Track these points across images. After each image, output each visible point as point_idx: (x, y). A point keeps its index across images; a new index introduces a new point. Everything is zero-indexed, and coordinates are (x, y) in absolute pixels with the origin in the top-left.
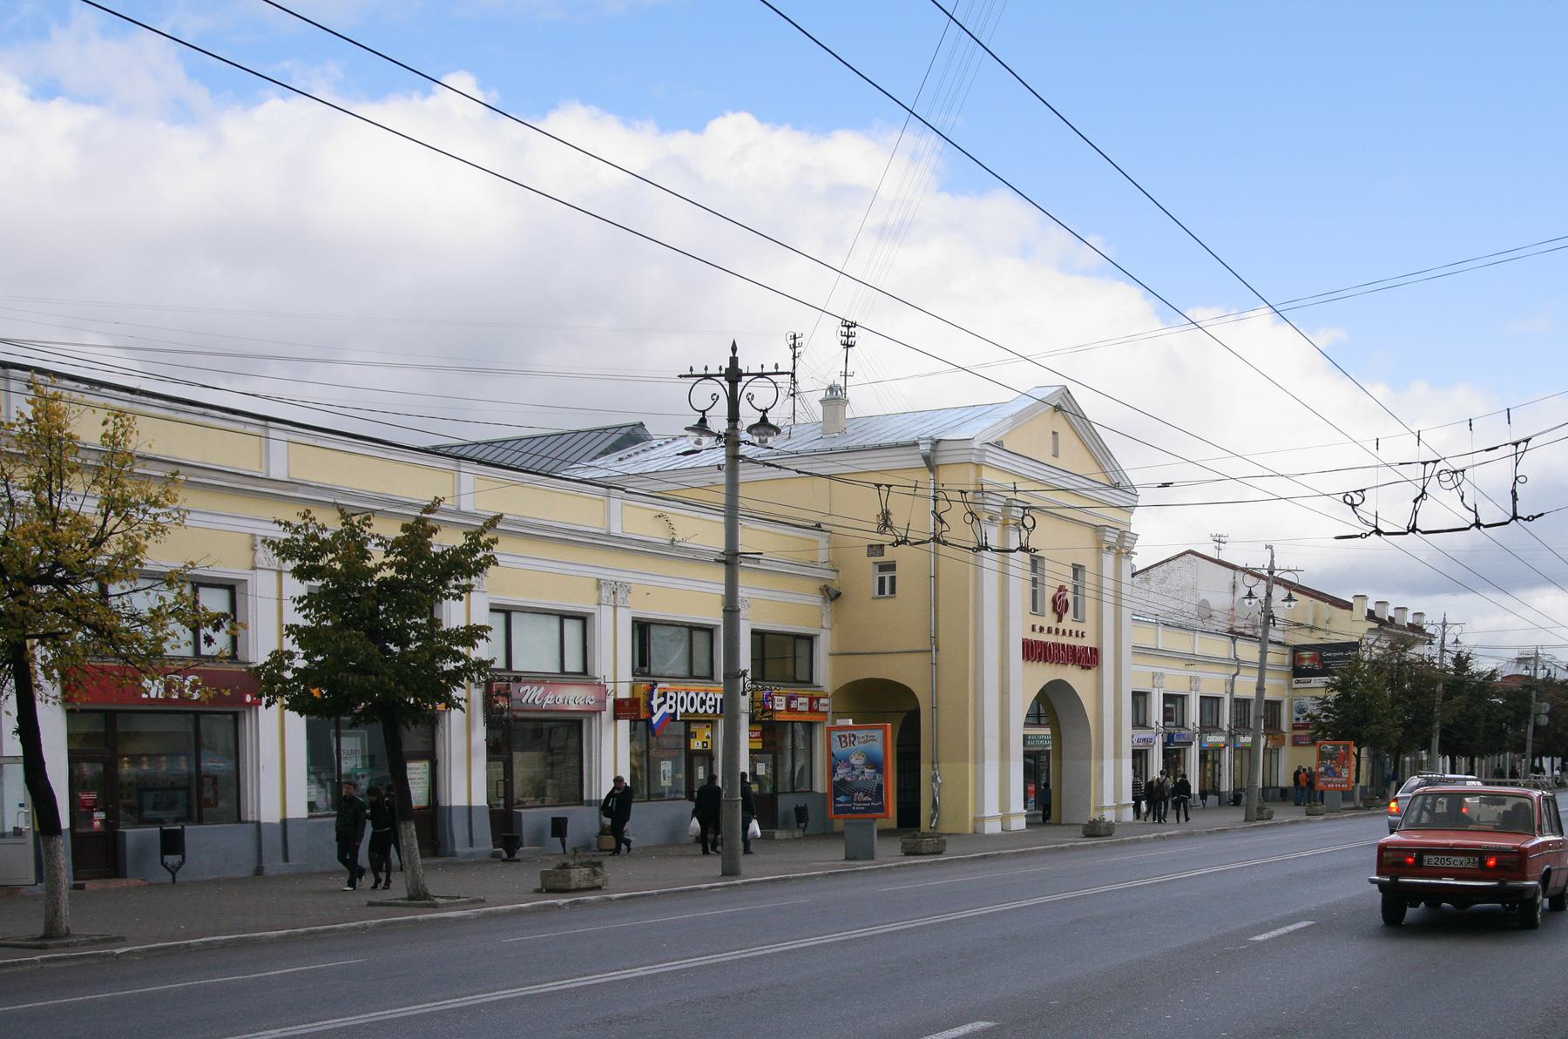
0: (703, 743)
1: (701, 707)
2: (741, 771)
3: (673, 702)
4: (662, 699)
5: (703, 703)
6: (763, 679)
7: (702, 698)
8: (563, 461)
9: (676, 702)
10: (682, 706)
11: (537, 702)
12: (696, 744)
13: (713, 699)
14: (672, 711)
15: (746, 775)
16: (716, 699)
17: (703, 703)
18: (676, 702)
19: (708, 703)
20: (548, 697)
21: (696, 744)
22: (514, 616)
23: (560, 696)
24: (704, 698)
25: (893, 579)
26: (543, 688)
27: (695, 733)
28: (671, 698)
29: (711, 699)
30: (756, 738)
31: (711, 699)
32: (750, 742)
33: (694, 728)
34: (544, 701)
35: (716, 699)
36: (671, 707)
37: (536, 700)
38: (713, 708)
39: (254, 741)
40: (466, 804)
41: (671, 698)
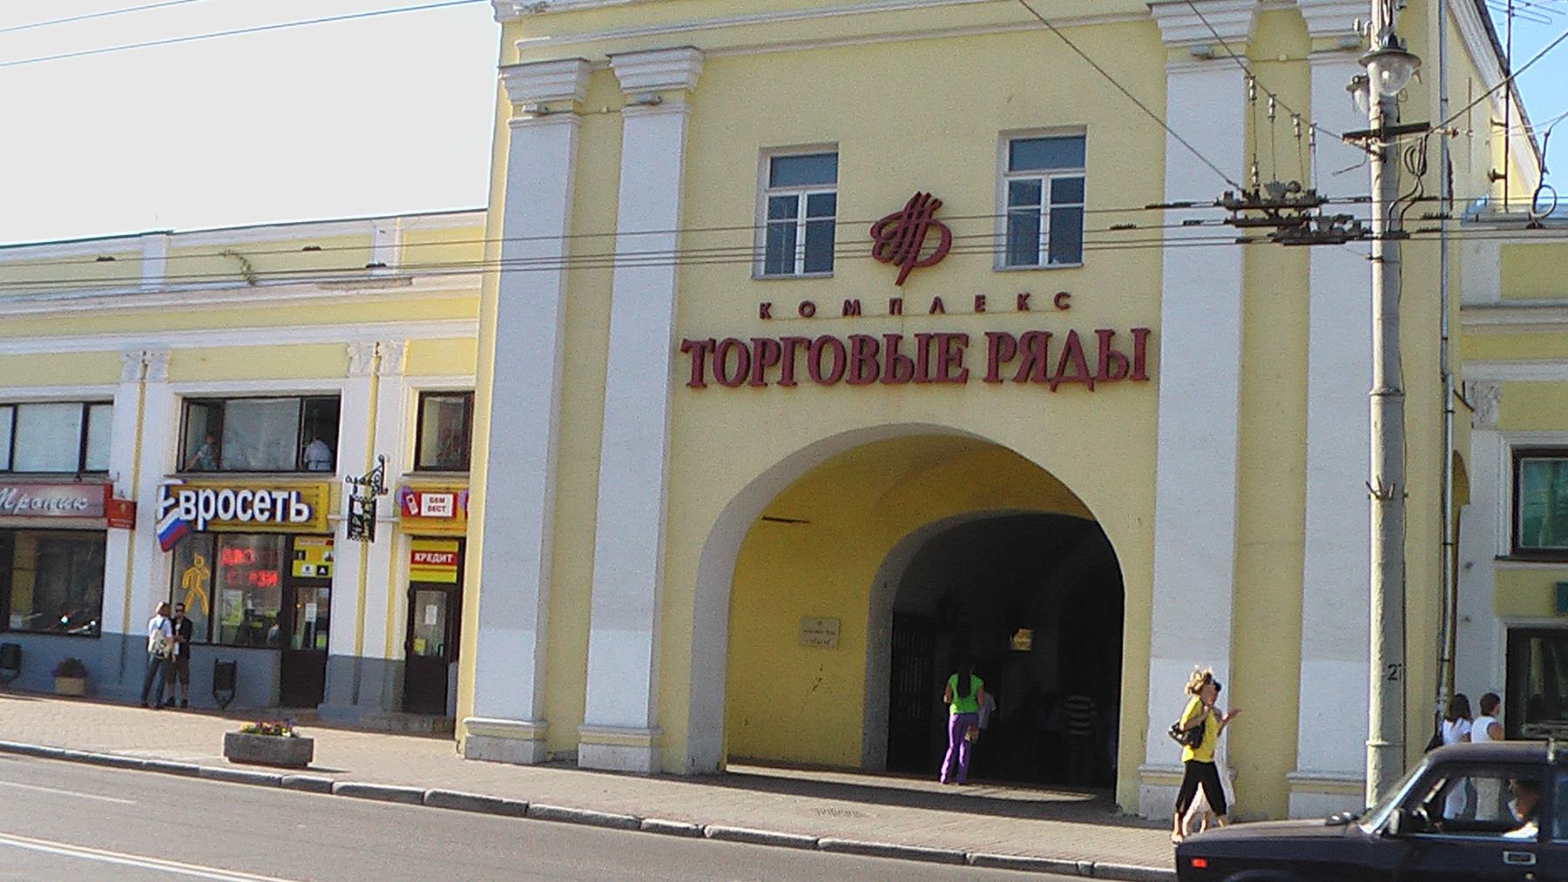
0: (319, 568)
1: (244, 511)
2: (307, 620)
3: (191, 505)
4: (172, 501)
5: (246, 505)
6: (216, 466)
7: (245, 499)
8: (1233, 56)
9: (196, 505)
10: (207, 509)
11: (7, 506)
12: (302, 569)
13: (268, 500)
14: (191, 517)
15: (1498, 699)
16: (274, 502)
17: (246, 505)
18: (196, 505)
19: (257, 505)
20: (21, 501)
21: (302, 569)
22: (22, 411)
23: (39, 501)
24: (250, 498)
25: (1070, 191)
26: (15, 490)
27: (304, 553)
28: (188, 499)
29: (262, 500)
30: (446, 563)
31: (262, 500)
32: (412, 570)
33: (299, 544)
34: (15, 506)
35: (274, 502)
36: (188, 511)
37: (7, 503)
38: (267, 514)
39: (1450, 565)
40: (121, 632)
41: (188, 499)
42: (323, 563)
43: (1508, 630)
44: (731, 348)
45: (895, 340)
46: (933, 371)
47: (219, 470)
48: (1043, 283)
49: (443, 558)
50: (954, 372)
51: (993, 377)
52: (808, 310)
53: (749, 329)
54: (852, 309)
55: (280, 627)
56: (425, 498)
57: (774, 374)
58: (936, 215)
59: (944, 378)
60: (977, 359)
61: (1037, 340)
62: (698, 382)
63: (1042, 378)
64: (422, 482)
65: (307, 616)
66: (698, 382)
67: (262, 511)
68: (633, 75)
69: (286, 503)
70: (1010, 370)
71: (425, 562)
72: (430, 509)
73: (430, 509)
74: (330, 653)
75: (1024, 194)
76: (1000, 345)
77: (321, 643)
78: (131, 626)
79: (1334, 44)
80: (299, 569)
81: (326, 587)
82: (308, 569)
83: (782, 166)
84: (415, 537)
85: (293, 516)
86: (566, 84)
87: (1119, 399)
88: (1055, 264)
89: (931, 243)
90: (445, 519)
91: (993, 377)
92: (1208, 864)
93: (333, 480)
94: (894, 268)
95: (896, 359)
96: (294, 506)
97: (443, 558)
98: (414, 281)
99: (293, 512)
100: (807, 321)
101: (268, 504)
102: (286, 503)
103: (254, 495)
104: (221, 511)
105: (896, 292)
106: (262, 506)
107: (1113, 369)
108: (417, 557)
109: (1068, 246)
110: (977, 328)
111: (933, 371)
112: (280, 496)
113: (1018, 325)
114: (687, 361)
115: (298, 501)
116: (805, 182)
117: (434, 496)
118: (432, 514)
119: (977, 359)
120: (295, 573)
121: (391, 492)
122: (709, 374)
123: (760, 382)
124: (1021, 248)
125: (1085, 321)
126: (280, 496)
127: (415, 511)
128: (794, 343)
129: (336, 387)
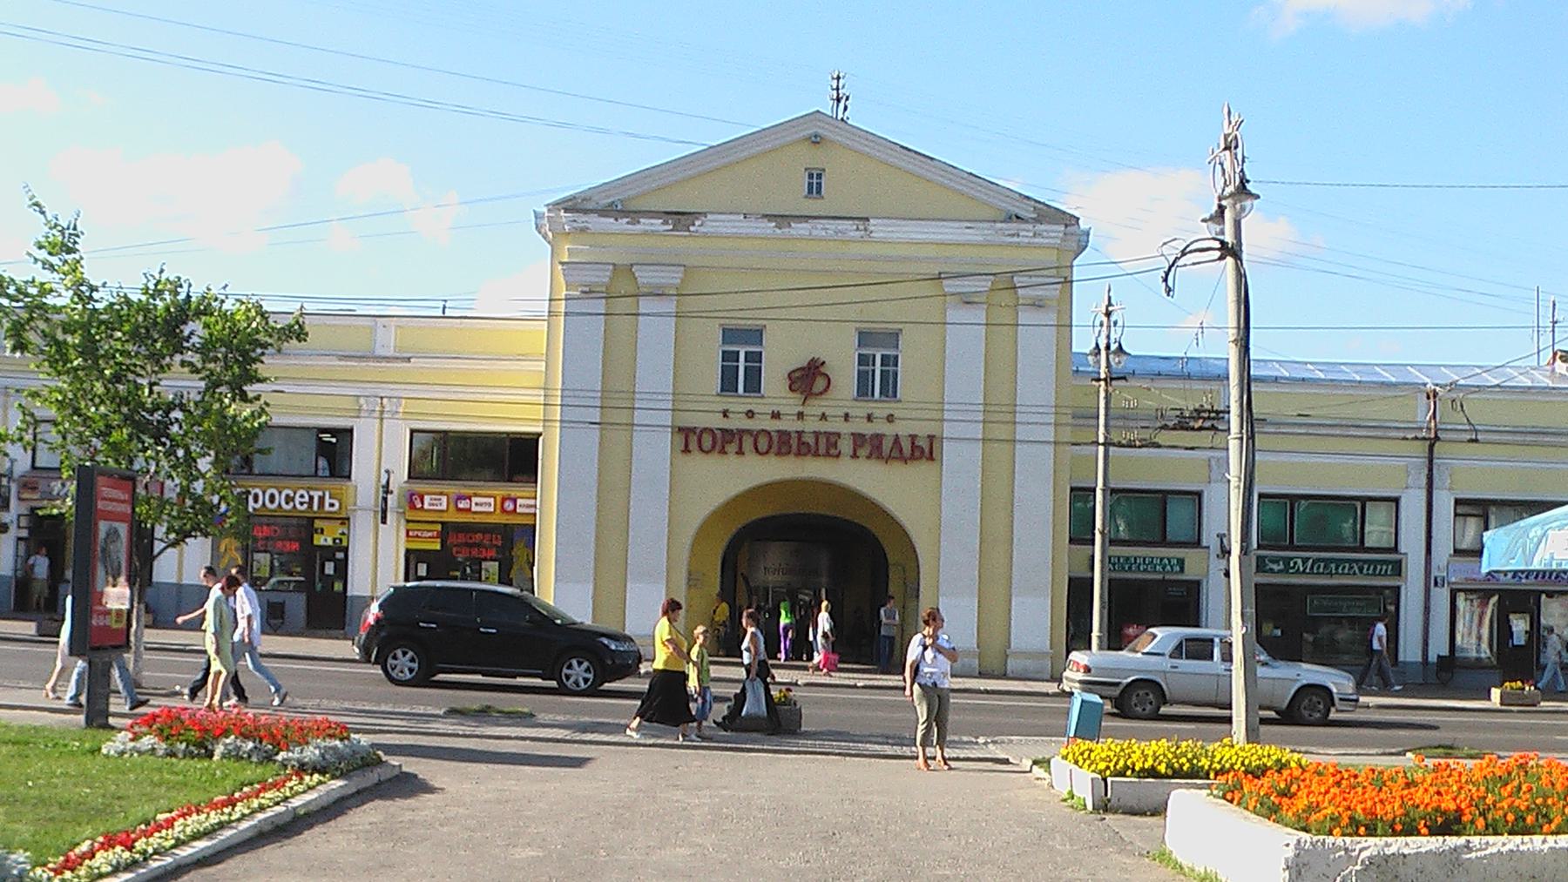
0: (334, 540)
1: (287, 503)
7: (287, 496)
16: (311, 498)
17: (289, 499)
19: (298, 499)
30: (433, 537)
33: (318, 524)
35: (311, 498)
38: (306, 506)
40: (174, 580)
42: (338, 536)
43: (1070, 579)
44: (765, 451)
45: (800, 433)
46: (822, 450)
47: (250, 473)
48: (881, 409)
49: (430, 534)
50: (833, 451)
51: (855, 456)
52: (750, 414)
53: (717, 422)
54: (776, 416)
55: (613, 651)
56: (427, 499)
57: (731, 448)
58: (822, 370)
59: (828, 455)
60: (846, 446)
61: (878, 438)
62: (686, 450)
63: (880, 457)
64: (419, 487)
65: (210, 543)
66: (686, 450)
67: (302, 504)
68: (645, 276)
69: (321, 499)
70: (863, 452)
71: (417, 536)
72: (430, 505)
73: (430, 505)
74: (349, 594)
75: (863, 360)
76: (859, 439)
77: (338, 586)
78: (185, 576)
79: (1029, 302)
80: (319, 541)
81: (428, 573)
82: (326, 540)
83: (730, 335)
84: (408, 521)
85: (327, 508)
86: (604, 277)
87: (922, 468)
88: (883, 398)
89: (820, 384)
90: (442, 511)
91: (855, 456)
92: (334, 555)
93: (349, 483)
94: (799, 396)
95: (801, 443)
96: (327, 501)
97: (430, 534)
98: (412, 360)
99: (327, 505)
100: (749, 421)
101: (306, 499)
102: (321, 499)
103: (295, 494)
104: (283, 503)
105: (801, 409)
106: (303, 500)
107: (917, 454)
108: (411, 534)
109: (890, 387)
110: (845, 428)
111: (822, 450)
112: (316, 495)
113: (868, 429)
114: (680, 439)
115: (330, 498)
116: (746, 343)
117: (434, 497)
118: (432, 508)
119: (846, 446)
120: (315, 542)
121: (395, 492)
122: (693, 445)
123: (723, 452)
124: (864, 389)
125: (903, 429)
126: (316, 495)
127: (419, 506)
128: (742, 432)
129: (351, 424)
